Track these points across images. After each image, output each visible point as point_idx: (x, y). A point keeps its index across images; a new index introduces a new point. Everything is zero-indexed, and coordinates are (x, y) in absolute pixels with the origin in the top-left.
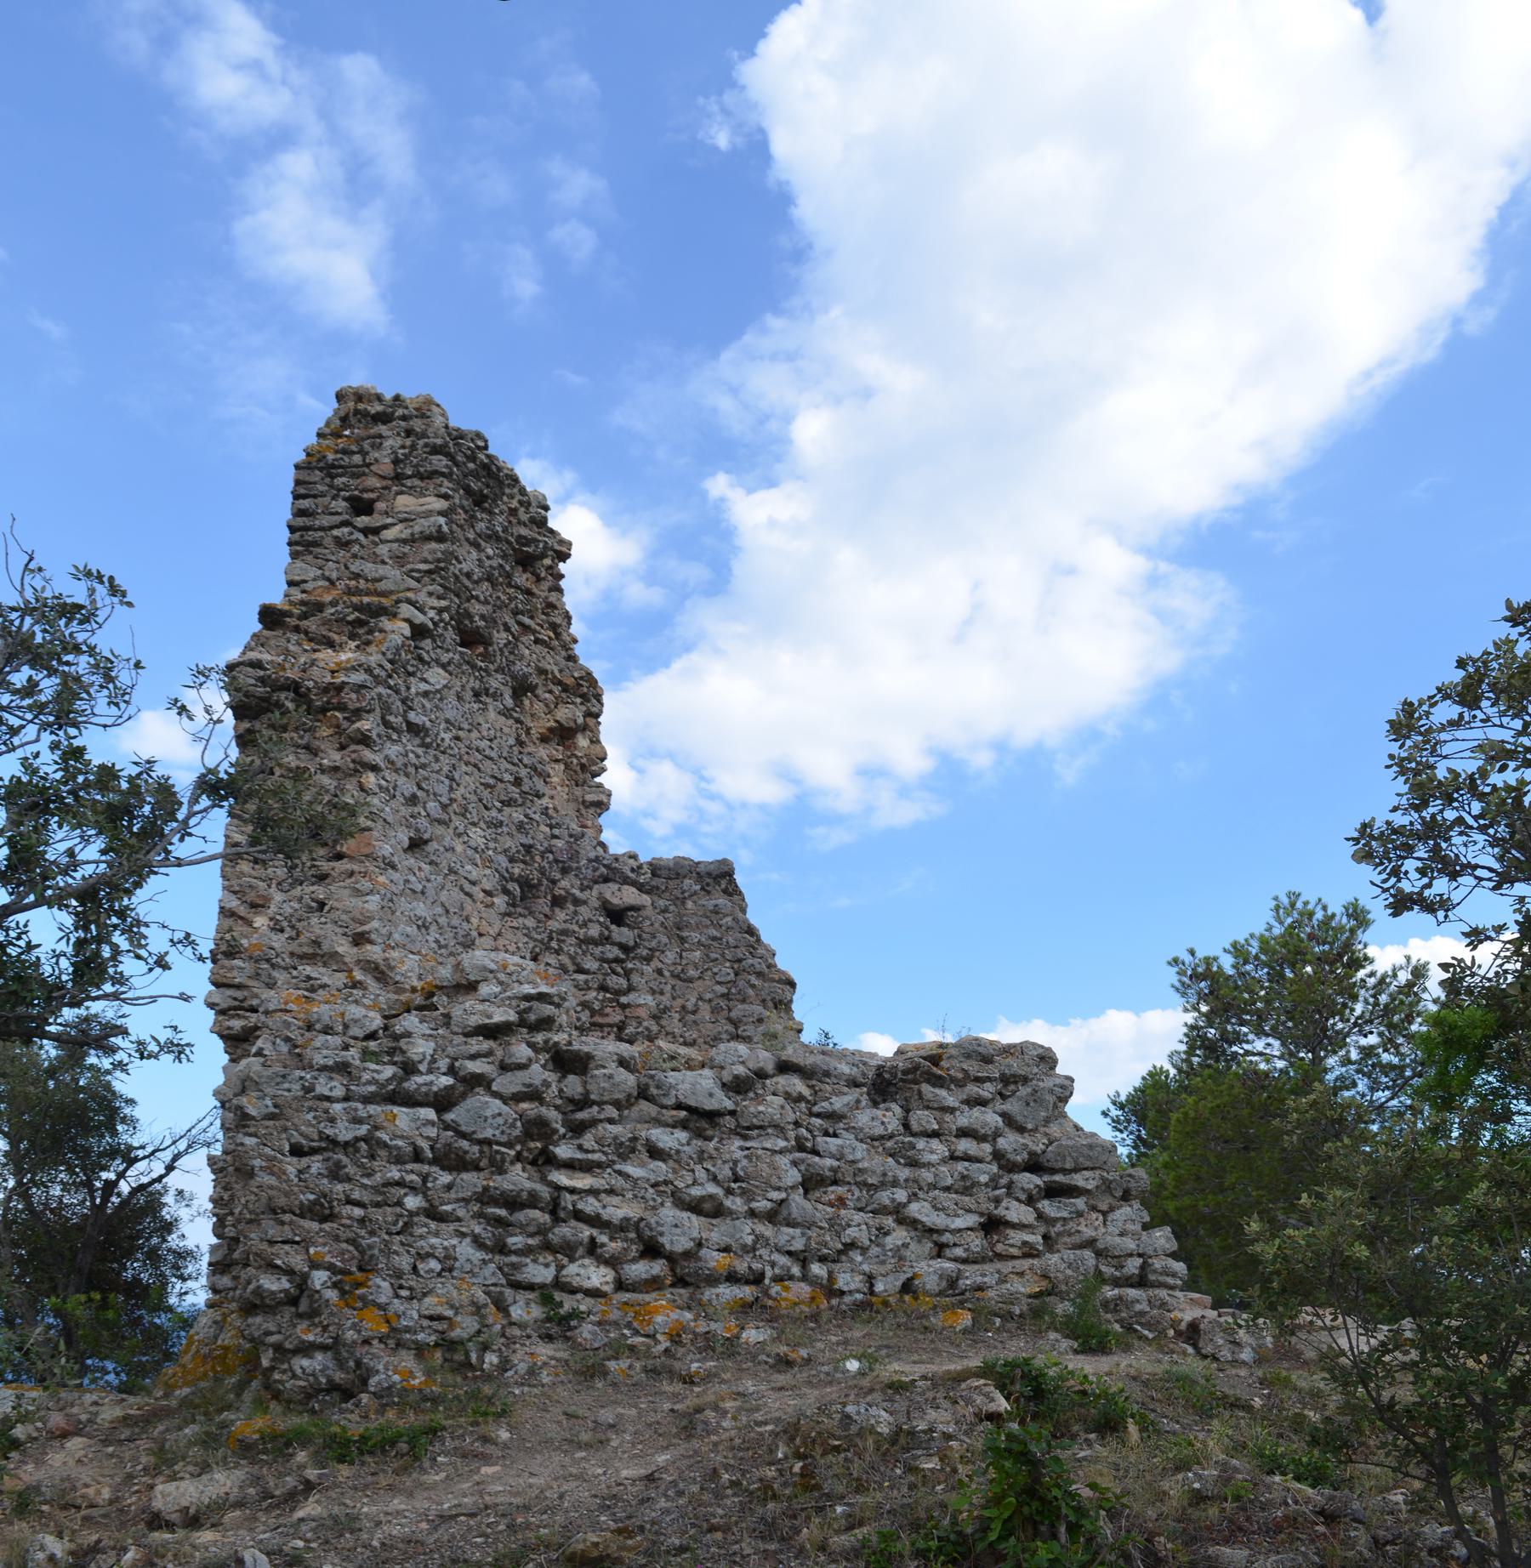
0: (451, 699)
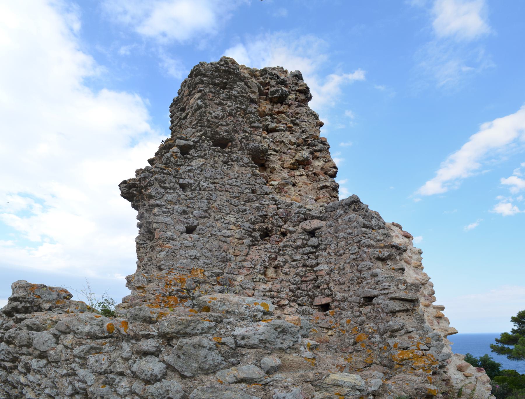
0: (208, 168)
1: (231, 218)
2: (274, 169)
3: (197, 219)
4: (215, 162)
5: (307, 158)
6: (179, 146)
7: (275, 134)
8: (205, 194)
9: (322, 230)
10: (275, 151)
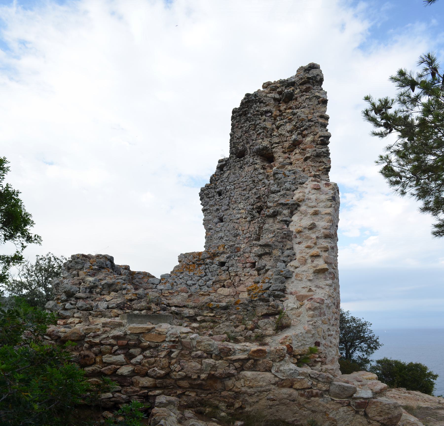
1: (241, 206)
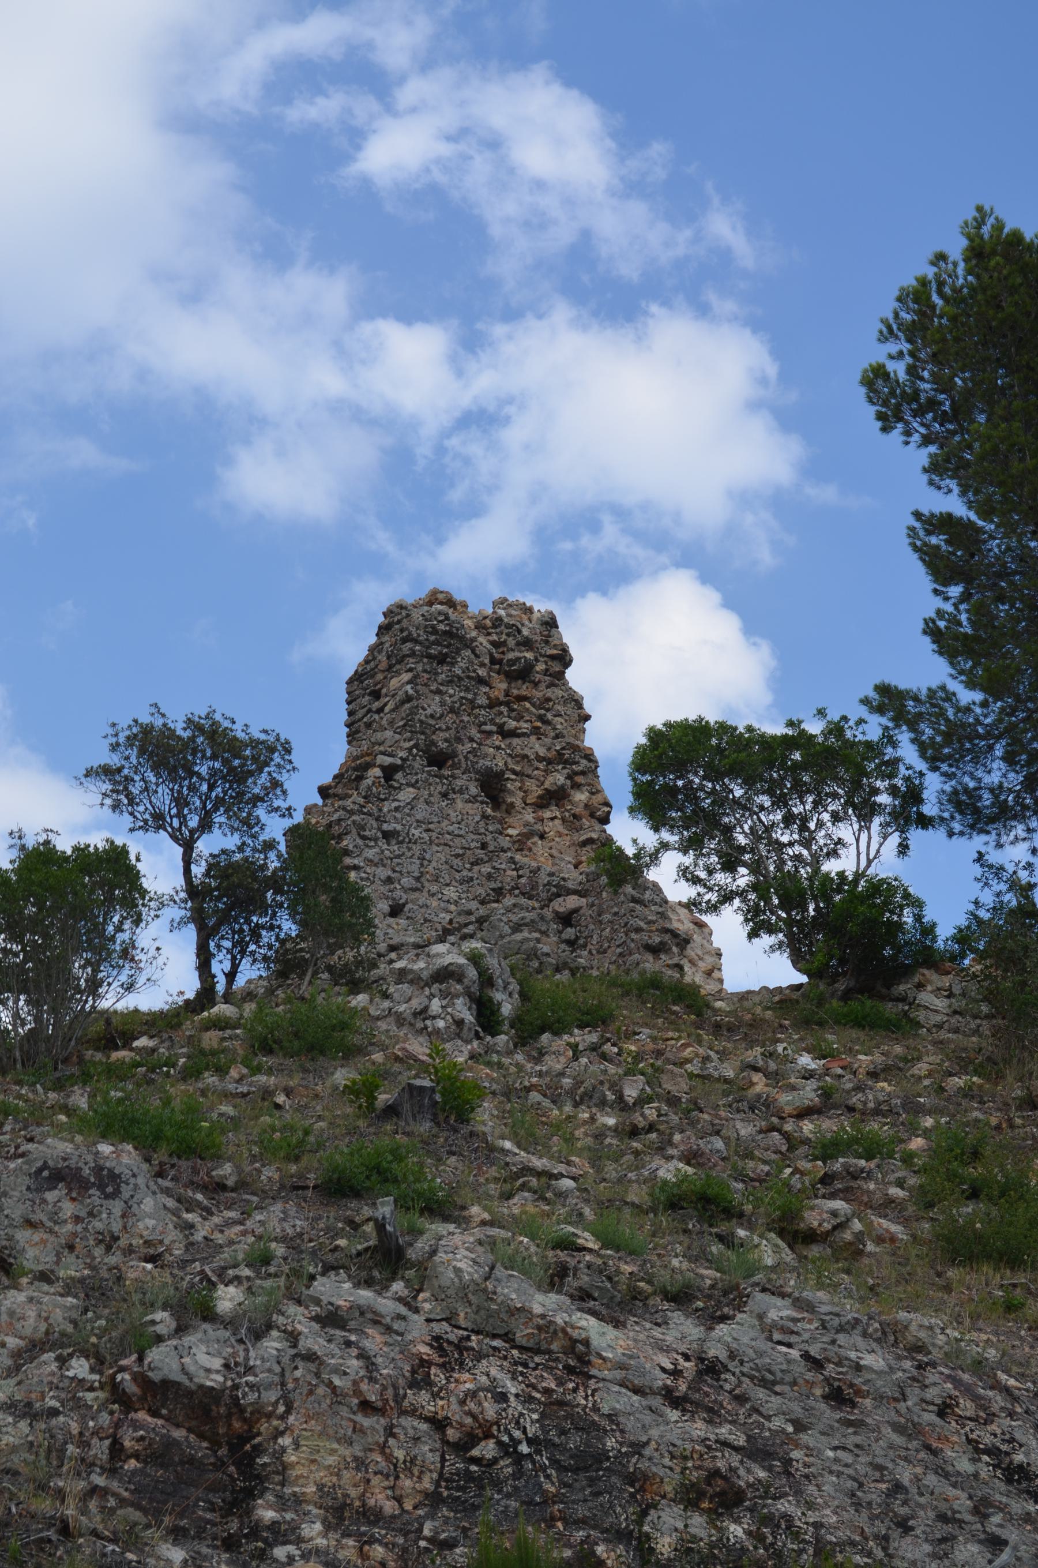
0: (421, 805)
1: (451, 893)
2: (512, 805)
3: (405, 892)
4: (430, 795)
5: (563, 786)
6: (381, 767)
7: (516, 741)
8: (416, 849)
9: (582, 912)
10: (514, 772)
